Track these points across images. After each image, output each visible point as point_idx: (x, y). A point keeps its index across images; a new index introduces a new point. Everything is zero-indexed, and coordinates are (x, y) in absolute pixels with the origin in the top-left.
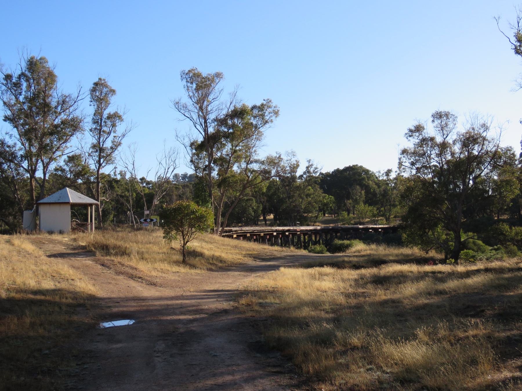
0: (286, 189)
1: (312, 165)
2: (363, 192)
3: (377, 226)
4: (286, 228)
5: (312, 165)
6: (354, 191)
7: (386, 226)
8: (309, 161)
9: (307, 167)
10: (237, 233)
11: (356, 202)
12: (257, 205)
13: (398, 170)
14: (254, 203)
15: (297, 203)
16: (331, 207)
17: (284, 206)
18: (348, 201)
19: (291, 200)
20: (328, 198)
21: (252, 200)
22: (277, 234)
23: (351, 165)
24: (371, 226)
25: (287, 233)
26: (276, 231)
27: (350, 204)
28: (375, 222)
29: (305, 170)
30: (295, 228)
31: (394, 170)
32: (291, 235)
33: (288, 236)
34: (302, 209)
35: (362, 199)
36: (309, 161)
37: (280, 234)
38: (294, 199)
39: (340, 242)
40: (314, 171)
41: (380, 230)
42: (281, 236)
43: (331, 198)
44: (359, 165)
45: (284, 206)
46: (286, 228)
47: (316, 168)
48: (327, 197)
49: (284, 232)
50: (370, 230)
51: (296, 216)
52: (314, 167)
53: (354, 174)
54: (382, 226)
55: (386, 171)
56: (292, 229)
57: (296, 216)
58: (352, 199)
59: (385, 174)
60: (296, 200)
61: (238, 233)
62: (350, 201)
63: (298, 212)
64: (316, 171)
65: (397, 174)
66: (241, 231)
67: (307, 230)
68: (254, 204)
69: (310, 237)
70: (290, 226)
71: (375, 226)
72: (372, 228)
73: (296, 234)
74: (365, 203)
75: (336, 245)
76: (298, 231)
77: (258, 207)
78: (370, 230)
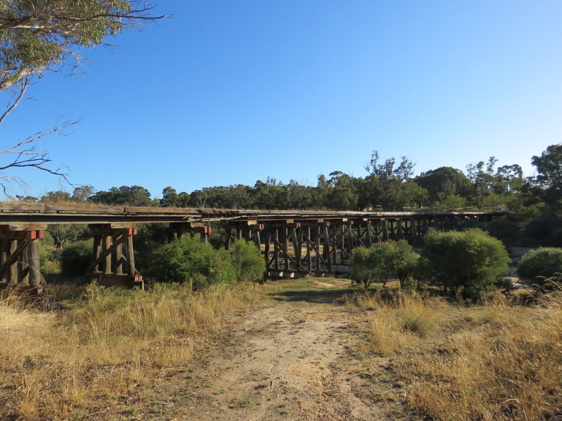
0: (383, 182)
1: (406, 161)
2: (454, 185)
3: (474, 213)
5: (406, 161)
7: (482, 213)
8: (404, 158)
9: (402, 164)
11: (448, 193)
13: (489, 162)
18: (440, 193)
20: (423, 191)
21: (348, 190)
23: (442, 167)
24: (466, 213)
25: (365, 220)
26: (346, 216)
27: (442, 195)
29: (400, 165)
31: (485, 163)
36: (404, 158)
38: (389, 190)
39: (441, 235)
40: (408, 166)
41: (475, 217)
47: (410, 164)
48: (421, 190)
50: (466, 217)
53: (445, 173)
54: (477, 213)
55: (477, 163)
58: (444, 191)
59: (476, 167)
60: (391, 191)
61: (259, 218)
62: (442, 193)
64: (410, 166)
65: (488, 166)
68: (351, 195)
69: (399, 223)
71: (471, 213)
72: (468, 215)
74: (456, 194)
75: (432, 240)
77: (355, 197)
78: (466, 217)
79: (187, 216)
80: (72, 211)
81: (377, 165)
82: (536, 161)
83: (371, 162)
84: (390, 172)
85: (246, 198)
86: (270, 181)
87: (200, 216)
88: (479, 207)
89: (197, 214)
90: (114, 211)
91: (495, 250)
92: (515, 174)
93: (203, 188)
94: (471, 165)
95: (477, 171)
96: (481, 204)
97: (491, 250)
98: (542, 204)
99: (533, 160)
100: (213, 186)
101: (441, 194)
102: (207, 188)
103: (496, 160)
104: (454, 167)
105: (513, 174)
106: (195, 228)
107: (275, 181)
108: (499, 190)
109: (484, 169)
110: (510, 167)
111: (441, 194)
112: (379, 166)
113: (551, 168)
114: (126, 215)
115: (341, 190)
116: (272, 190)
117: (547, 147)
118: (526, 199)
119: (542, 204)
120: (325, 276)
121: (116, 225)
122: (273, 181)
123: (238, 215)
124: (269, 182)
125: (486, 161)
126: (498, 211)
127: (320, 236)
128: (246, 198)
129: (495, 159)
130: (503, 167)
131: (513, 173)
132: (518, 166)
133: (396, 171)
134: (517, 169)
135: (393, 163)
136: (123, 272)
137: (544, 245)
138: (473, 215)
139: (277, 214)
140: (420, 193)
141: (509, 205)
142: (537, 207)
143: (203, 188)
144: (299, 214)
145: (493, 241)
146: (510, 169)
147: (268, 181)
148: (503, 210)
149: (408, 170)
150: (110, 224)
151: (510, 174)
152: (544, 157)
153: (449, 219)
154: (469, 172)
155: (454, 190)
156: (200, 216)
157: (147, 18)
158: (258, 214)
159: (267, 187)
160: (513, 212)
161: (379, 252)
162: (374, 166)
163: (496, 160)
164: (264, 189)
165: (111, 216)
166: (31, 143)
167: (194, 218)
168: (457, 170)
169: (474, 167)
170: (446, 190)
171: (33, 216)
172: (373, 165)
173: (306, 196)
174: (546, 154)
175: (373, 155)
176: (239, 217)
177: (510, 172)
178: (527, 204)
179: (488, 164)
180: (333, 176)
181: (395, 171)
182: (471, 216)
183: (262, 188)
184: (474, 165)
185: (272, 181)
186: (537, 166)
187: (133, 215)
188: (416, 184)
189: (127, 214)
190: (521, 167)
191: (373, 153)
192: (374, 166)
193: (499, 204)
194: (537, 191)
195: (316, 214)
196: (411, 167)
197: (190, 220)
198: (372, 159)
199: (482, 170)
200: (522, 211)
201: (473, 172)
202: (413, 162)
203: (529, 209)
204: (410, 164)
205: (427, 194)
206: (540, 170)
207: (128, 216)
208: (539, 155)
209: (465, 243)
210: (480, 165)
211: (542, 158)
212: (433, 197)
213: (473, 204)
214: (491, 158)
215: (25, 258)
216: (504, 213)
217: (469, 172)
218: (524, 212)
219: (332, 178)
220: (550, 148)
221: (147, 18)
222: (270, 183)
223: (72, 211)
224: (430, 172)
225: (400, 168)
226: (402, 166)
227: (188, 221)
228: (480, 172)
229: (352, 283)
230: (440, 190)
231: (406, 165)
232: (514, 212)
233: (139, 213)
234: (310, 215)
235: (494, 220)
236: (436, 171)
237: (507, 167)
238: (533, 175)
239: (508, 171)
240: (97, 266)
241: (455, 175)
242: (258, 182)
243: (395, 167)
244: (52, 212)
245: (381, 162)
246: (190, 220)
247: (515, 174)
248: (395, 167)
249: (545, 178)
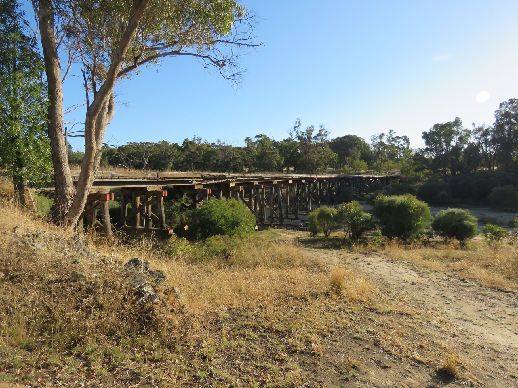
0: (303, 147)
1: (323, 129)
3: (375, 176)
4: (303, 176)
5: (323, 129)
6: (353, 151)
8: (321, 126)
9: (320, 131)
10: (236, 181)
11: (354, 158)
12: (280, 158)
13: (389, 134)
14: (278, 156)
15: (311, 157)
16: (336, 162)
17: (301, 160)
18: (348, 158)
19: (307, 155)
20: (334, 155)
22: (293, 181)
25: (304, 181)
26: (292, 178)
27: (349, 160)
28: (198, 197)
30: (312, 176)
31: (386, 134)
32: (308, 183)
33: (304, 184)
34: (315, 162)
35: (358, 156)
36: (321, 126)
37: (297, 182)
38: (309, 154)
39: (387, 199)
41: (371, 179)
42: (297, 184)
43: (335, 155)
44: (353, 135)
45: (301, 160)
46: (303, 176)
47: (326, 132)
49: (300, 179)
51: (310, 167)
52: (325, 130)
54: (379, 176)
55: (379, 134)
56: (309, 176)
57: (310, 167)
59: (378, 137)
61: (236, 181)
62: (349, 158)
63: (312, 164)
65: (388, 137)
66: (242, 177)
67: (323, 179)
68: (278, 157)
70: (306, 174)
72: (373, 178)
73: (312, 182)
76: (315, 179)
77: (281, 159)
79: (192, 180)
80: (127, 177)
81: (299, 132)
82: (426, 136)
83: (294, 129)
84: (309, 139)
85: (177, 155)
86: (196, 139)
87: (202, 180)
88: (379, 171)
89: (199, 178)
90: (151, 176)
91: (425, 210)
92: (404, 144)
93: (128, 143)
94: (374, 135)
95: (379, 140)
96: (380, 169)
97: (423, 210)
98: (428, 171)
99: (423, 135)
100: (138, 141)
101: (348, 159)
102: (131, 143)
103: (394, 133)
104: (358, 136)
105: (402, 144)
106: (198, 189)
107: (201, 139)
108: (392, 156)
109: (385, 140)
110: (401, 138)
111: (348, 159)
112: (301, 132)
113: (436, 142)
114: (158, 179)
115: (270, 152)
116: (200, 148)
117: (433, 125)
118: (416, 166)
119: (428, 171)
120: (277, 228)
121: (150, 188)
122: (199, 140)
123: (225, 178)
124: (195, 140)
125: (387, 133)
126: (393, 175)
127: (274, 195)
128: (177, 155)
129: (393, 132)
130: (395, 138)
131: (402, 143)
132: (407, 137)
133: (315, 137)
134: (406, 140)
135: (312, 130)
136: (153, 226)
137: (451, 207)
138: (376, 178)
139: (249, 177)
140: (331, 157)
141: (402, 171)
142: (423, 173)
143: (128, 143)
144: (262, 177)
145: (423, 204)
146: (400, 139)
147: (194, 139)
148: (397, 174)
149: (324, 137)
150: (147, 187)
151: (400, 143)
152: (432, 133)
153: (359, 181)
154: (372, 141)
155: (360, 155)
156: (202, 180)
157: (250, 45)
158: (236, 177)
159: (194, 146)
160: (404, 176)
161: (345, 210)
162: (297, 132)
163: (394, 133)
164: (192, 147)
165: (149, 180)
166: (68, 113)
167: (197, 181)
168: (361, 138)
169: (377, 137)
170: (353, 155)
171: (101, 182)
172: (296, 131)
173: (236, 156)
174: (433, 130)
175: (296, 122)
176: (226, 180)
177: (400, 141)
178: (417, 171)
179: (387, 135)
180: (257, 138)
181: (314, 138)
182: (375, 179)
183: (190, 145)
184: (376, 136)
185: (197, 140)
186: (425, 139)
187: (162, 179)
188: (329, 149)
189: (159, 179)
190: (409, 138)
191: (296, 120)
192: (297, 132)
193: (392, 168)
194: (426, 161)
195: (273, 177)
196: (326, 135)
197: (194, 183)
198: (295, 126)
199: (383, 140)
200: (411, 175)
201: (375, 141)
202: (329, 131)
203: (418, 174)
204: (326, 132)
205: (338, 158)
206: (427, 143)
207: (159, 180)
208: (428, 131)
209: (407, 205)
210: (381, 136)
211: (429, 134)
212: (342, 161)
213: (374, 168)
214: (390, 130)
215: (95, 216)
216: (398, 177)
217: (372, 141)
218: (412, 177)
219: (257, 140)
220: (436, 126)
221: (250, 45)
222: (196, 141)
223: (127, 177)
224: (339, 138)
225: (318, 135)
226: (320, 134)
227: (193, 184)
228: (381, 142)
229: (311, 234)
230: (348, 155)
231: (323, 133)
232: (405, 177)
233: (166, 178)
234: (269, 177)
235: (391, 183)
236: (343, 138)
237: (398, 138)
238: (422, 148)
239: (398, 140)
240: (125, 222)
241: (359, 142)
242: (186, 140)
243: (314, 134)
244: (115, 178)
245: (303, 129)
246: (194, 183)
247: (404, 144)
248: (314, 134)
249: (431, 150)
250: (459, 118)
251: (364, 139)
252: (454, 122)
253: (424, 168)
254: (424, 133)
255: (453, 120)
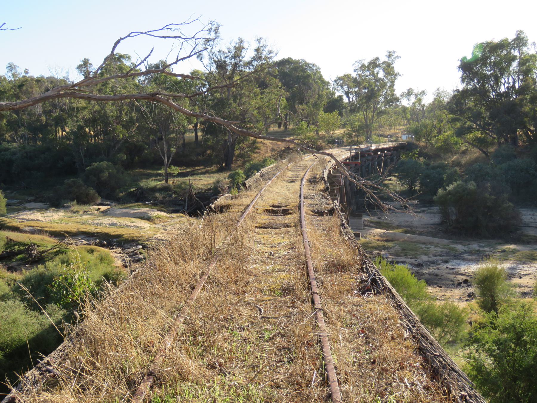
1: (264, 46)
18: (300, 107)
41: (379, 153)
47: (270, 52)
52: (266, 49)
103: (398, 57)
116: (509, 244)
118: (458, 125)
129: (396, 55)
163: (398, 57)
168: (313, 65)
192: (211, 52)
204: (270, 52)
208: (469, 57)
214: (389, 52)
250: (522, 32)
251: (320, 67)
252: (514, 40)
253: (470, 129)
254: (88, 60)
255: (511, 37)
